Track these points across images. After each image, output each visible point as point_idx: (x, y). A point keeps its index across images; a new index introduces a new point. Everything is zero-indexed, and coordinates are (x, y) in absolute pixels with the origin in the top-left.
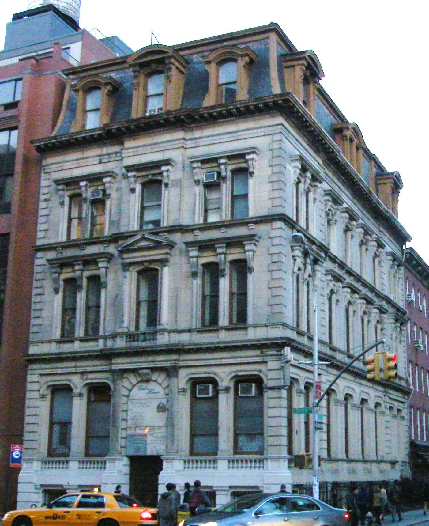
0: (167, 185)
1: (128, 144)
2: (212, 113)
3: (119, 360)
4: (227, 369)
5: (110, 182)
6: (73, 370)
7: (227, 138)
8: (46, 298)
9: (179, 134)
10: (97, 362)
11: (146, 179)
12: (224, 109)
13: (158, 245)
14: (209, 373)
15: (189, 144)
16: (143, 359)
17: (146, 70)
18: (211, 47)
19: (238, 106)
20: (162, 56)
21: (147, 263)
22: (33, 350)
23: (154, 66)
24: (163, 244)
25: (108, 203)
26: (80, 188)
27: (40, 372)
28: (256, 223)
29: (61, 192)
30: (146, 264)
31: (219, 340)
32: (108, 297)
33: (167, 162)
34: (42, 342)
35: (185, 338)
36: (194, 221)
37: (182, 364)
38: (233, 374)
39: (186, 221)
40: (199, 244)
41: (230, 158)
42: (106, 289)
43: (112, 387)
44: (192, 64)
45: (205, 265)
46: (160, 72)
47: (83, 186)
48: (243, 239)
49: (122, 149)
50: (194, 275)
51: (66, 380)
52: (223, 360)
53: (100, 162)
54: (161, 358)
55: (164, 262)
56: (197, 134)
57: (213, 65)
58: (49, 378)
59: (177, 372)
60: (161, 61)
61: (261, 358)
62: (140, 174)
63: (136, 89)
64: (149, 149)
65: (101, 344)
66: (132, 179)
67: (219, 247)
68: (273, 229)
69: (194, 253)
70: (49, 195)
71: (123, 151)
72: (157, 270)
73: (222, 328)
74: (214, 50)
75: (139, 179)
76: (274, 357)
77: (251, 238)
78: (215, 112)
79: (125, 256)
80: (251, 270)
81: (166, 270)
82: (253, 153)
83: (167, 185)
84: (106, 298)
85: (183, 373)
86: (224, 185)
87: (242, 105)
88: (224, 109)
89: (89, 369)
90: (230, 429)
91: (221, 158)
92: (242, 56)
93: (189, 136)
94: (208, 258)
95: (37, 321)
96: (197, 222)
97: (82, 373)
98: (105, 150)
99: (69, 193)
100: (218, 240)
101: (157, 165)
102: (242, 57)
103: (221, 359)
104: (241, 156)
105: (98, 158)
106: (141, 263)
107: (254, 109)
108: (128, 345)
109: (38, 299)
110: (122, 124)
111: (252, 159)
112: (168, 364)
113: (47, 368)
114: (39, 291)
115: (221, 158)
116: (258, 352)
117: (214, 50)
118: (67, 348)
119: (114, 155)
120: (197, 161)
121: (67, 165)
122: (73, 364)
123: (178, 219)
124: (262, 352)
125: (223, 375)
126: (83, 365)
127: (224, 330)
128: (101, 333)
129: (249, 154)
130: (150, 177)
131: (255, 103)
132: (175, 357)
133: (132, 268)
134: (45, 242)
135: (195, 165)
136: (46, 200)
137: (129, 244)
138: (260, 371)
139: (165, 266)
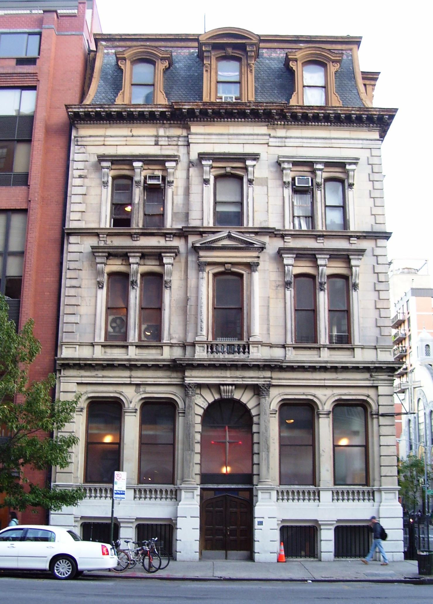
0: (250, 182)
1: (194, 129)
2: (307, 114)
3: (195, 373)
4: (328, 392)
5: (173, 168)
6: (127, 381)
7: (319, 143)
8: (83, 292)
9: (263, 130)
10: (160, 374)
11: (222, 172)
12: (323, 111)
13: (248, 246)
14: (306, 395)
15: (273, 142)
16: (228, 373)
17: (221, 53)
18: (129, 43)
19: (339, 112)
20: (244, 41)
21: (229, 265)
22: (66, 353)
23: (230, 51)
24: (255, 246)
25: (169, 191)
26: (133, 169)
27: (79, 380)
28: (358, 237)
29: (106, 170)
30: (228, 266)
31: (127, 357)
32: (173, 299)
33: (255, 157)
34: (81, 345)
35: (278, 353)
36: (284, 227)
37: (274, 382)
38: (337, 398)
39: (274, 223)
40: (296, 252)
41: (328, 164)
42: (170, 289)
43: (181, 404)
44: (261, 59)
45: (111, 275)
46: (238, 59)
47: (138, 167)
48: (316, 252)
49: (188, 134)
50: (287, 285)
51: (116, 392)
52: (326, 381)
53: (157, 144)
54: (252, 374)
55: (251, 267)
56: (281, 132)
57: (128, 63)
58: (90, 388)
59: (268, 391)
60: (242, 47)
61: (372, 382)
62: (216, 165)
63: (207, 71)
64: (225, 139)
65: (167, 354)
66: (207, 169)
67: (321, 258)
68: (377, 247)
69: (288, 260)
70: (86, 171)
71: (189, 136)
72: (241, 276)
73: (324, 346)
74: (130, 47)
75: (212, 170)
76: (386, 382)
77: (361, 252)
78: (311, 113)
79: (202, 253)
80: (355, 286)
81: (256, 276)
82: (355, 164)
83: (250, 182)
84: (170, 301)
85: (273, 392)
86: (319, 192)
87: (343, 112)
88: (323, 111)
89: (150, 381)
90: (331, 457)
91: (317, 163)
92: (163, 59)
93: (273, 133)
94: (116, 266)
95: (71, 319)
96: (102, 226)
97: (138, 385)
98: (161, 132)
99: (112, 173)
100: (321, 251)
101: (242, 158)
102: (333, 62)
103: (325, 380)
104: (342, 165)
105: (154, 139)
106: (223, 264)
107: (148, 116)
108: (211, 356)
109: (72, 292)
110: (197, 105)
111: (354, 170)
112: (260, 382)
113: (87, 376)
114: (74, 283)
115: (317, 163)
116: (367, 375)
117: (130, 47)
118: (117, 354)
119: (176, 139)
120: (288, 162)
121: (109, 141)
122: (127, 373)
123: (265, 221)
124: (371, 376)
125: (323, 399)
126: (139, 376)
127: (326, 349)
128: (165, 340)
129: (350, 164)
130: (228, 170)
131: (358, 113)
132: (268, 374)
133: (208, 269)
134: (82, 225)
135: (104, 164)
136: (80, 177)
137: (209, 241)
138: (368, 396)
139: (255, 271)
